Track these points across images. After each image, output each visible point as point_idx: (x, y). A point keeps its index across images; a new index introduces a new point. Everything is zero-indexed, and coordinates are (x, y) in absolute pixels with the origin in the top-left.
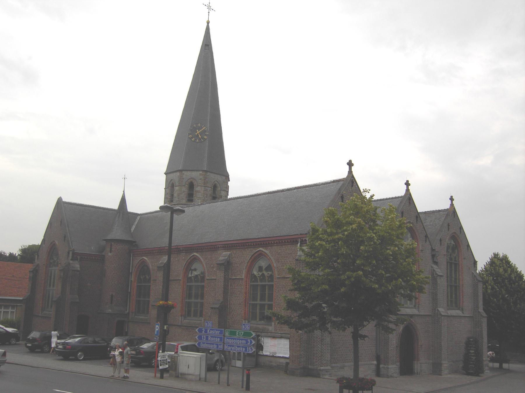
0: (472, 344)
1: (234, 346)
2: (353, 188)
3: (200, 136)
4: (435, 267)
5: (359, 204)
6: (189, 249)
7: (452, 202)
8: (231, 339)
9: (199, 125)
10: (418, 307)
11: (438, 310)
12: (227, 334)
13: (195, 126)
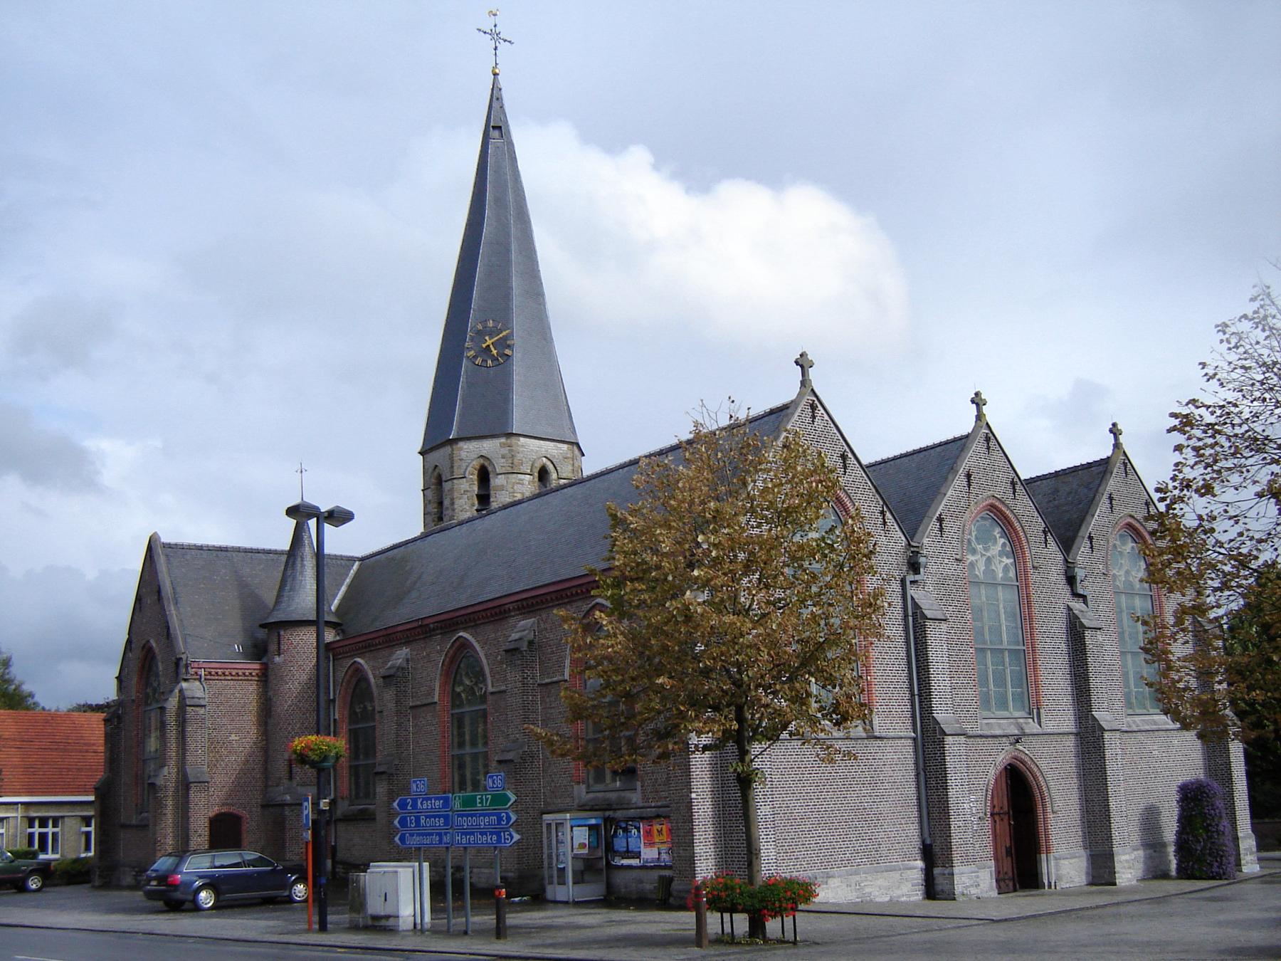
0: (1197, 803)
1: (473, 833)
2: (1130, 477)
3: (495, 352)
4: (1077, 606)
5: (832, 460)
6: (449, 623)
7: (1116, 438)
8: (467, 816)
9: (491, 324)
10: (1039, 714)
11: (1094, 719)
12: (457, 805)
13: (480, 327)
